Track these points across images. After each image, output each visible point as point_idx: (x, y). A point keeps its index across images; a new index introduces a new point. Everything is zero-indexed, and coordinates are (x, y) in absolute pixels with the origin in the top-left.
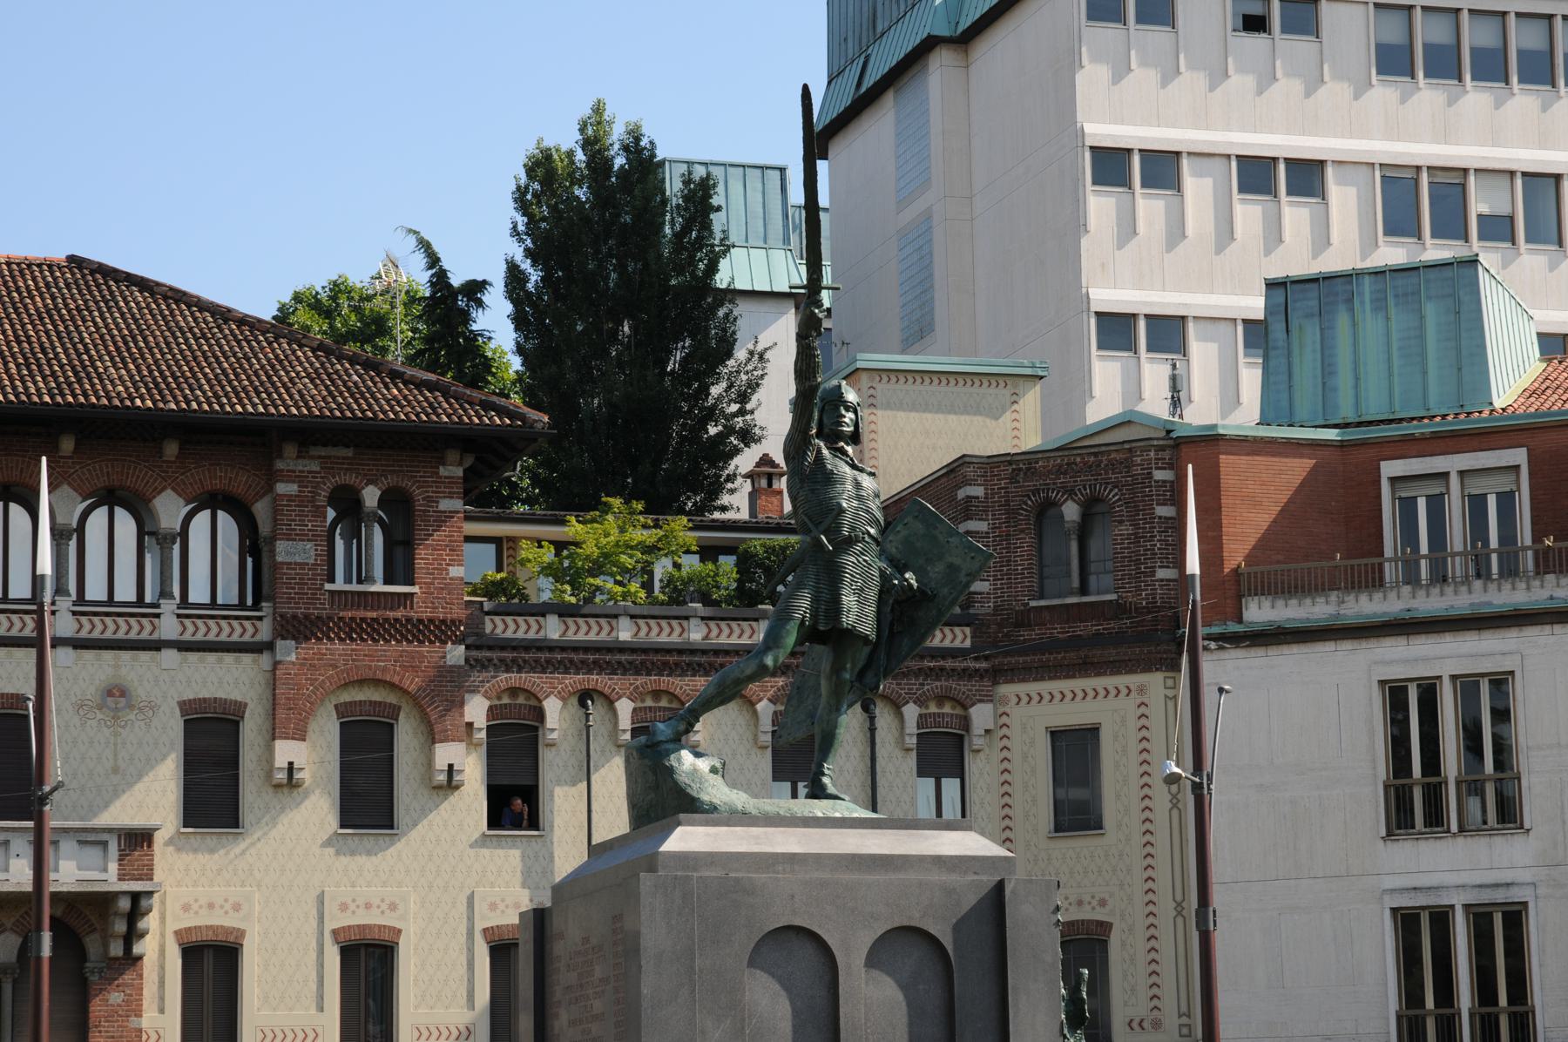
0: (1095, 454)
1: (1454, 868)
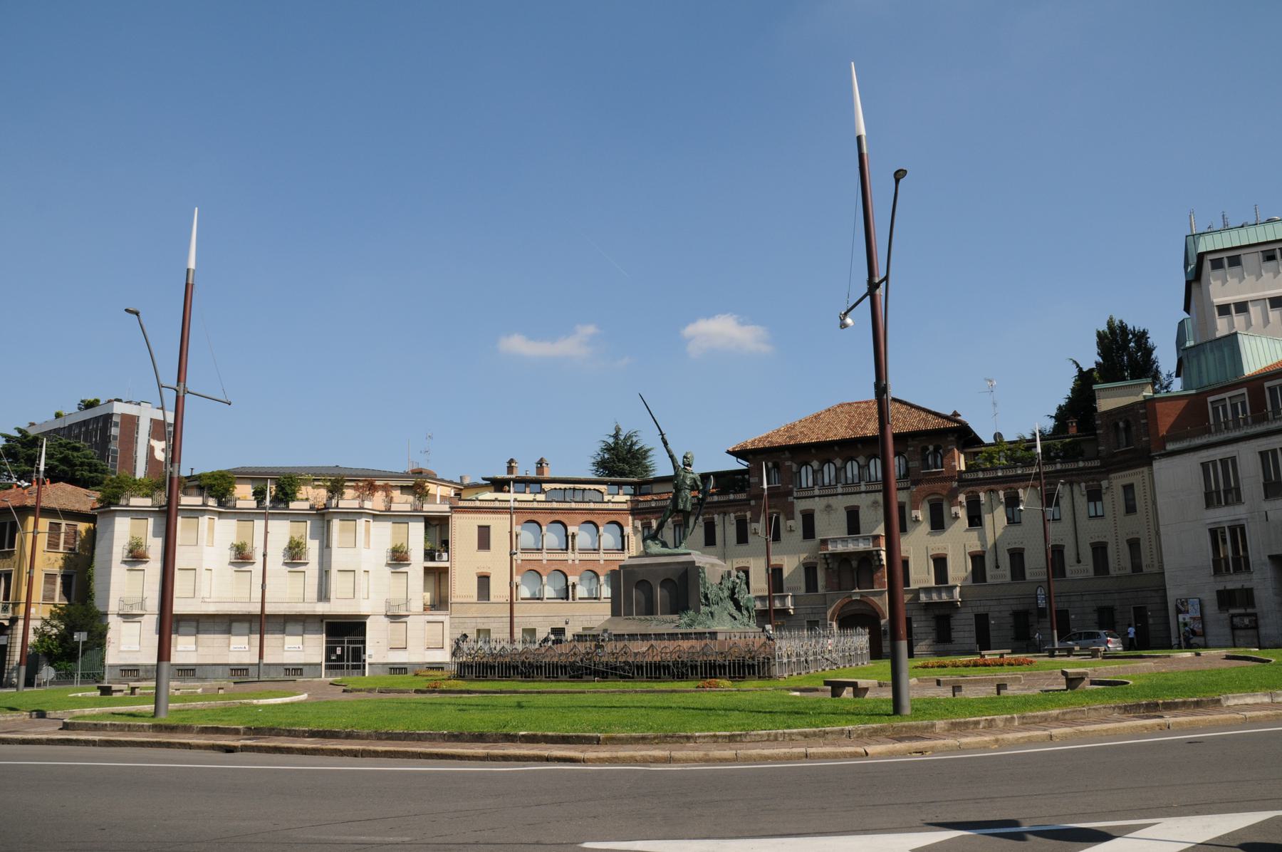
1: (1224, 515)
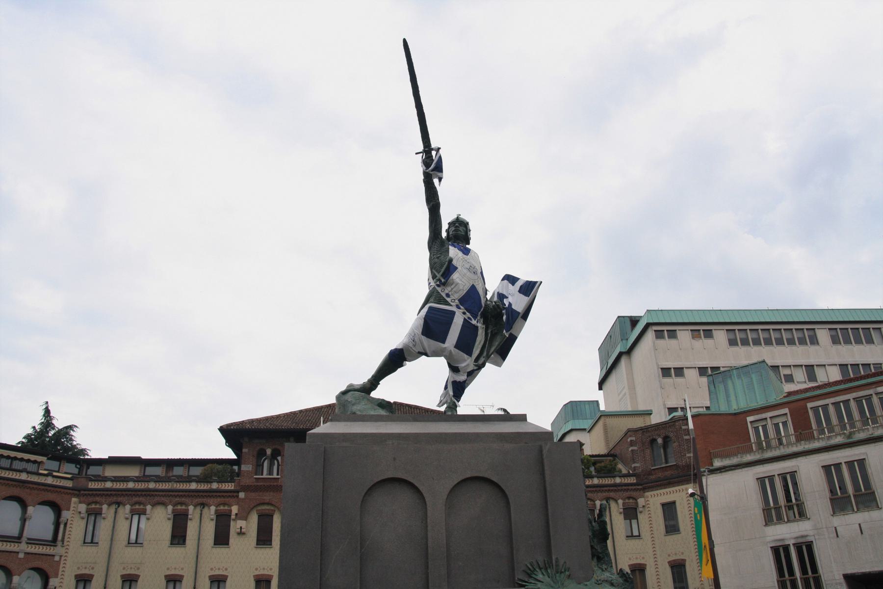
1: (787, 532)
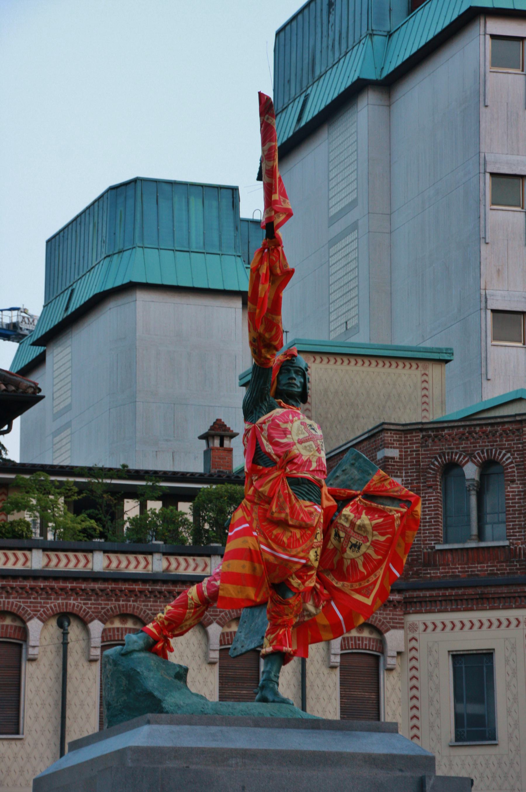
0: (492, 425)
